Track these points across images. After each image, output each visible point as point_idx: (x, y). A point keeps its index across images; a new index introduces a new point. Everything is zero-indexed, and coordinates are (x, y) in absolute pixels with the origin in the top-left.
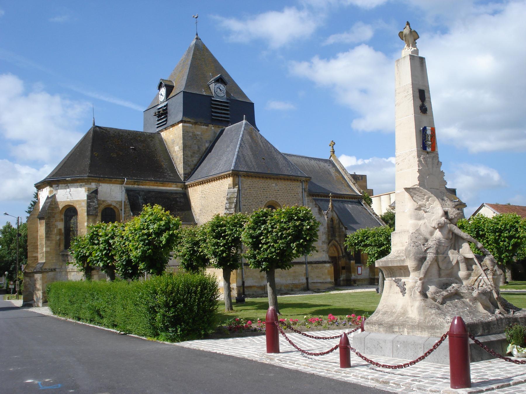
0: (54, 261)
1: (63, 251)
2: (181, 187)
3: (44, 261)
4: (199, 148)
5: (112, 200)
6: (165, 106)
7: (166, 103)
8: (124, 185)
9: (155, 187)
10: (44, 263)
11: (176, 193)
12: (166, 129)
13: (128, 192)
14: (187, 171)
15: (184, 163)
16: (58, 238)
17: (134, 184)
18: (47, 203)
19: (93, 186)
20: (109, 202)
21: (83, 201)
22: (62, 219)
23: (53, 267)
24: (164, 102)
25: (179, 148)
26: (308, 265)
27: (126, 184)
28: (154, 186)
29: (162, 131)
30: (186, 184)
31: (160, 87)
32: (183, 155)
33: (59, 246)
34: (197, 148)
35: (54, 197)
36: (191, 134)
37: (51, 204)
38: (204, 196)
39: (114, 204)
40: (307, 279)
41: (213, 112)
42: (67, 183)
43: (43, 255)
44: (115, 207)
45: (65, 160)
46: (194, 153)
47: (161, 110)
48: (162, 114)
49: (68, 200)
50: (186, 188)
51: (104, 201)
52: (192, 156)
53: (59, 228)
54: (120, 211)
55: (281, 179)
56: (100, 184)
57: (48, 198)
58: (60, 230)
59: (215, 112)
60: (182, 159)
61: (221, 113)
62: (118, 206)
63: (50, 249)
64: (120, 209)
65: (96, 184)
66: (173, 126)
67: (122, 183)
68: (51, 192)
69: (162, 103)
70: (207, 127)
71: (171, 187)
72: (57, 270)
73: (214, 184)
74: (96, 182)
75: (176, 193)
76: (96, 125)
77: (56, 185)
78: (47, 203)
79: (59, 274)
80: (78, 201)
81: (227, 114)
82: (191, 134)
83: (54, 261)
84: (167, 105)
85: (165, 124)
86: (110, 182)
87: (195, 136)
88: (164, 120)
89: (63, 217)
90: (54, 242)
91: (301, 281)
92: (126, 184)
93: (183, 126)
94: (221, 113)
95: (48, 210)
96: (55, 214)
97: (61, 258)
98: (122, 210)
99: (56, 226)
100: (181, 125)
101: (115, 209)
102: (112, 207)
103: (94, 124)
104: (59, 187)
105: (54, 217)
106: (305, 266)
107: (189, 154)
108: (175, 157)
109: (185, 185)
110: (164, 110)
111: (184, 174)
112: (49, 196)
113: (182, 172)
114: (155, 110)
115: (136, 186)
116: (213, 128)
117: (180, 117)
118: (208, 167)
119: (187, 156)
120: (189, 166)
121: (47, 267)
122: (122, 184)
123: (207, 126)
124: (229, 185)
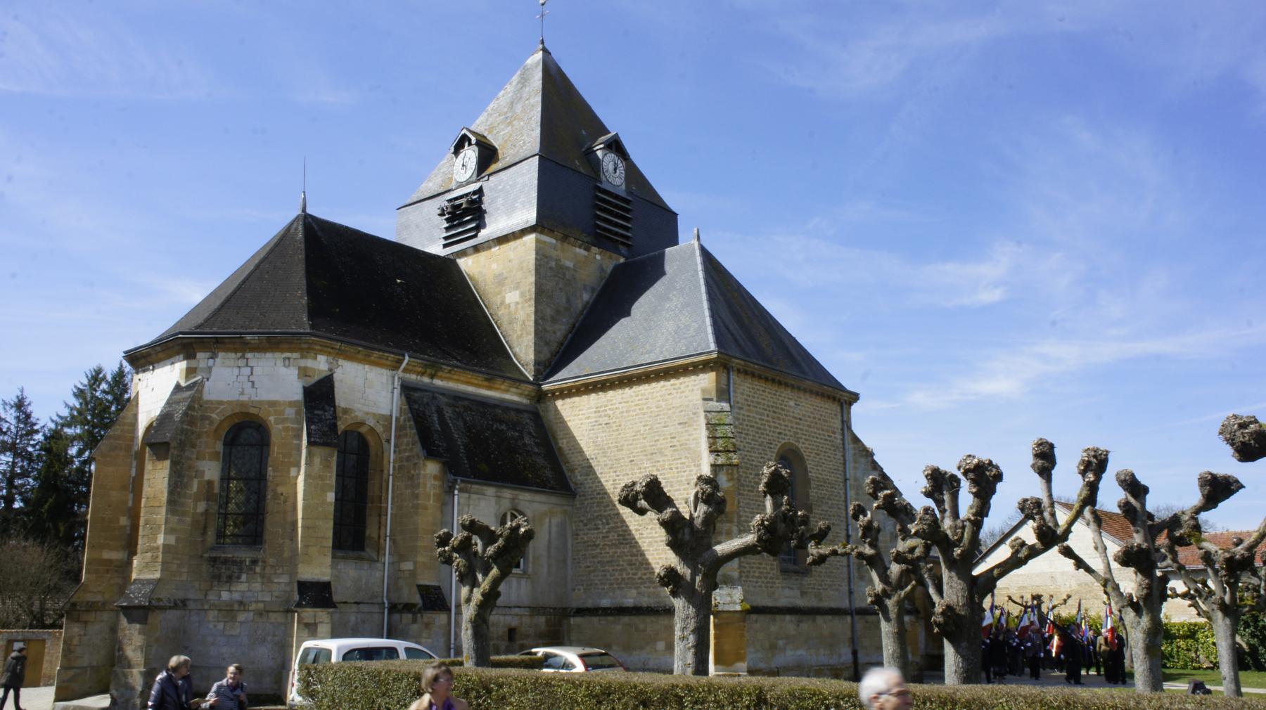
0: (184, 577)
1: (212, 549)
2: (527, 396)
3: (157, 575)
4: (568, 300)
5: (366, 409)
6: (475, 193)
7: (475, 187)
8: (400, 373)
9: (470, 389)
10: (159, 580)
11: (518, 409)
12: (476, 249)
13: (408, 390)
14: (542, 358)
15: (536, 333)
16: (201, 507)
17: (423, 374)
18: (178, 403)
19: (321, 364)
20: (359, 415)
21: (291, 404)
22: (218, 453)
23: (180, 595)
24: (468, 183)
25: (522, 295)
26: (857, 618)
27: (405, 370)
28: (468, 383)
29: (463, 253)
30: (546, 387)
31: (458, 148)
32: (536, 312)
33: (204, 532)
34: (564, 300)
35: (196, 387)
36: (553, 264)
37: (190, 408)
38: (604, 420)
39: (371, 422)
40: (855, 653)
41: (599, 218)
42: (244, 351)
43: (154, 559)
44: (372, 429)
45: (230, 291)
46: (558, 312)
47: (463, 201)
48: (466, 212)
49: (245, 398)
50: (541, 397)
51: (346, 411)
52: (554, 320)
53: (207, 478)
54: (385, 444)
55: (805, 391)
56: (341, 362)
57: (178, 388)
58: (210, 483)
59: (605, 220)
60: (532, 323)
61: (617, 225)
62: (379, 429)
63: (177, 540)
64: (384, 437)
65: (330, 359)
66: (503, 240)
67: (395, 367)
68: (190, 372)
69: (461, 185)
70: (585, 253)
71: (507, 391)
72: (192, 605)
73: (645, 389)
74: (329, 354)
75: (518, 411)
76: (309, 211)
77: (208, 355)
78: (178, 403)
79: (195, 618)
80: (273, 404)
81: (626, 229)
82: (553, 264)
83: (184, 577)
84: (480, 191)
85: (475, 236)
86: (366, 360)
87: (560, 271)
88: (473, 225)
89: (219, 447)
90: (188, 519)
91: (843, 659)
92: (405, 370)
93: (538, 241)
94: (617, 225)
95: (182, 422)
96: (199, 436)
97: (205, 568)
98: (388, 441)
99: (199, 474)
100: (531, 238)
101: (369, 438)
102: (363, 430)
103: (304, 210)
104: (218, 360)
105: (194, 446)
106: (849, 618)
107: (549, 312)
108: (505, 321)
109: (540, 390)
110: (472, 202)
111: (537, 363)
112: (183, 384)
113: (532, 357)
114: (442, 202)
115: (426, 380)
116: (598, 257)
117: (529, 216)
118: (617, 346)
119: (543, 318)
120: (547, 344)
121: (164, 594)
122: (396, 368)
123: (587, 249)
124: (703, 391)
